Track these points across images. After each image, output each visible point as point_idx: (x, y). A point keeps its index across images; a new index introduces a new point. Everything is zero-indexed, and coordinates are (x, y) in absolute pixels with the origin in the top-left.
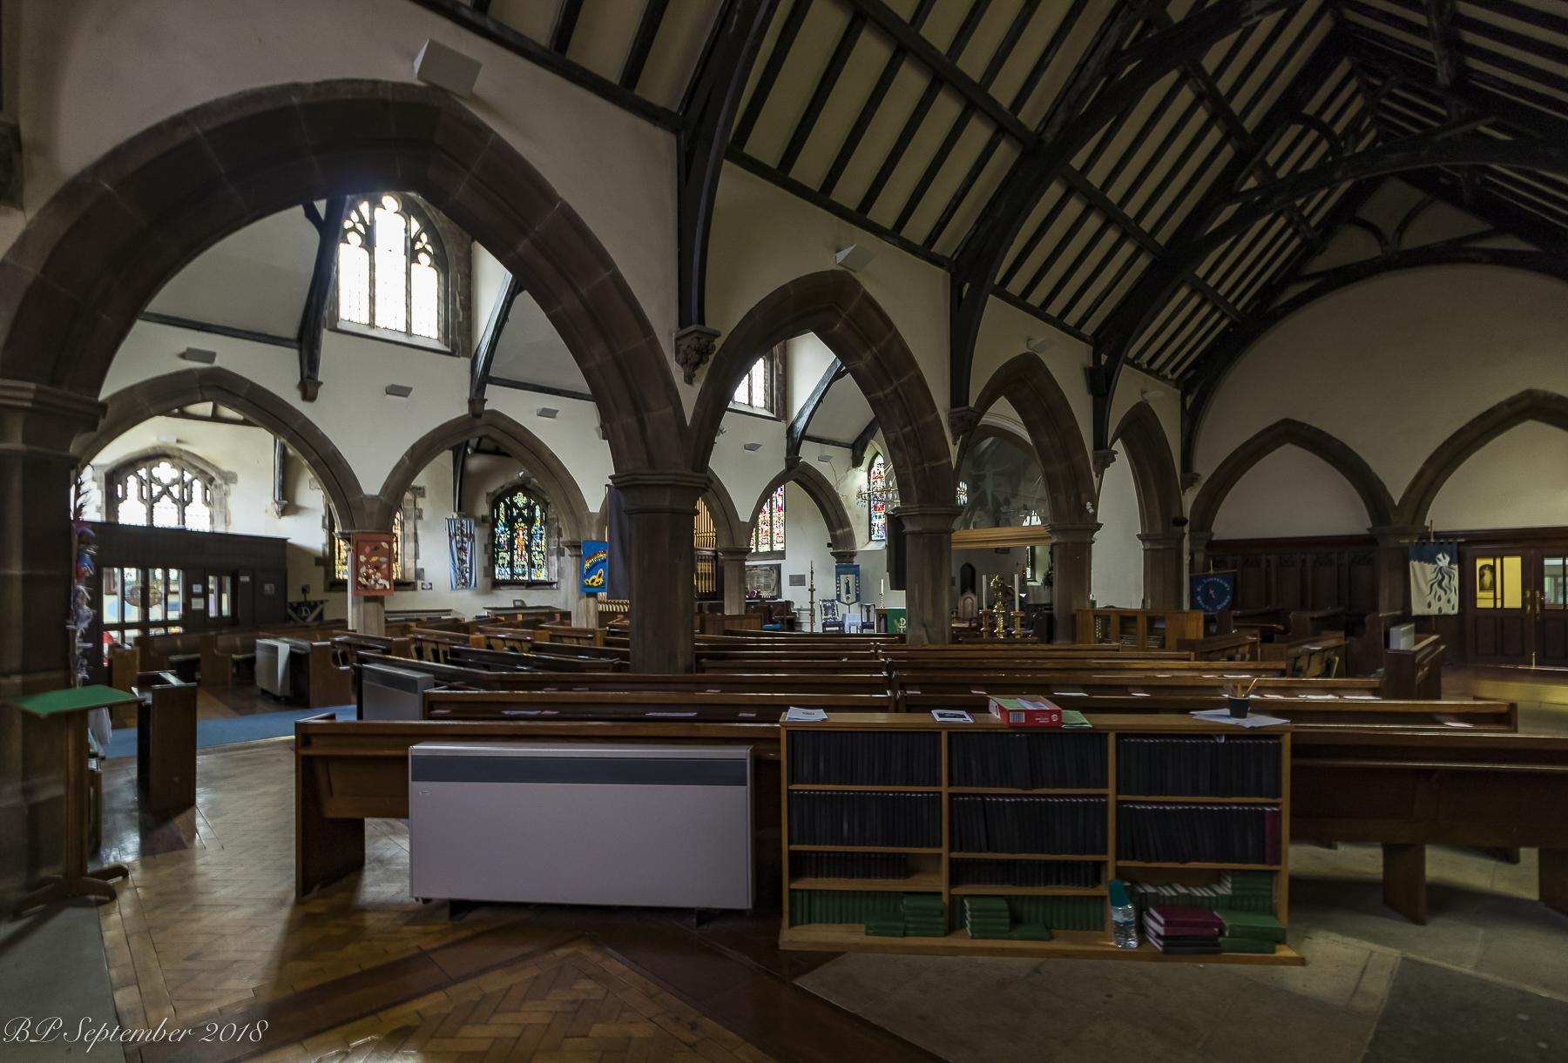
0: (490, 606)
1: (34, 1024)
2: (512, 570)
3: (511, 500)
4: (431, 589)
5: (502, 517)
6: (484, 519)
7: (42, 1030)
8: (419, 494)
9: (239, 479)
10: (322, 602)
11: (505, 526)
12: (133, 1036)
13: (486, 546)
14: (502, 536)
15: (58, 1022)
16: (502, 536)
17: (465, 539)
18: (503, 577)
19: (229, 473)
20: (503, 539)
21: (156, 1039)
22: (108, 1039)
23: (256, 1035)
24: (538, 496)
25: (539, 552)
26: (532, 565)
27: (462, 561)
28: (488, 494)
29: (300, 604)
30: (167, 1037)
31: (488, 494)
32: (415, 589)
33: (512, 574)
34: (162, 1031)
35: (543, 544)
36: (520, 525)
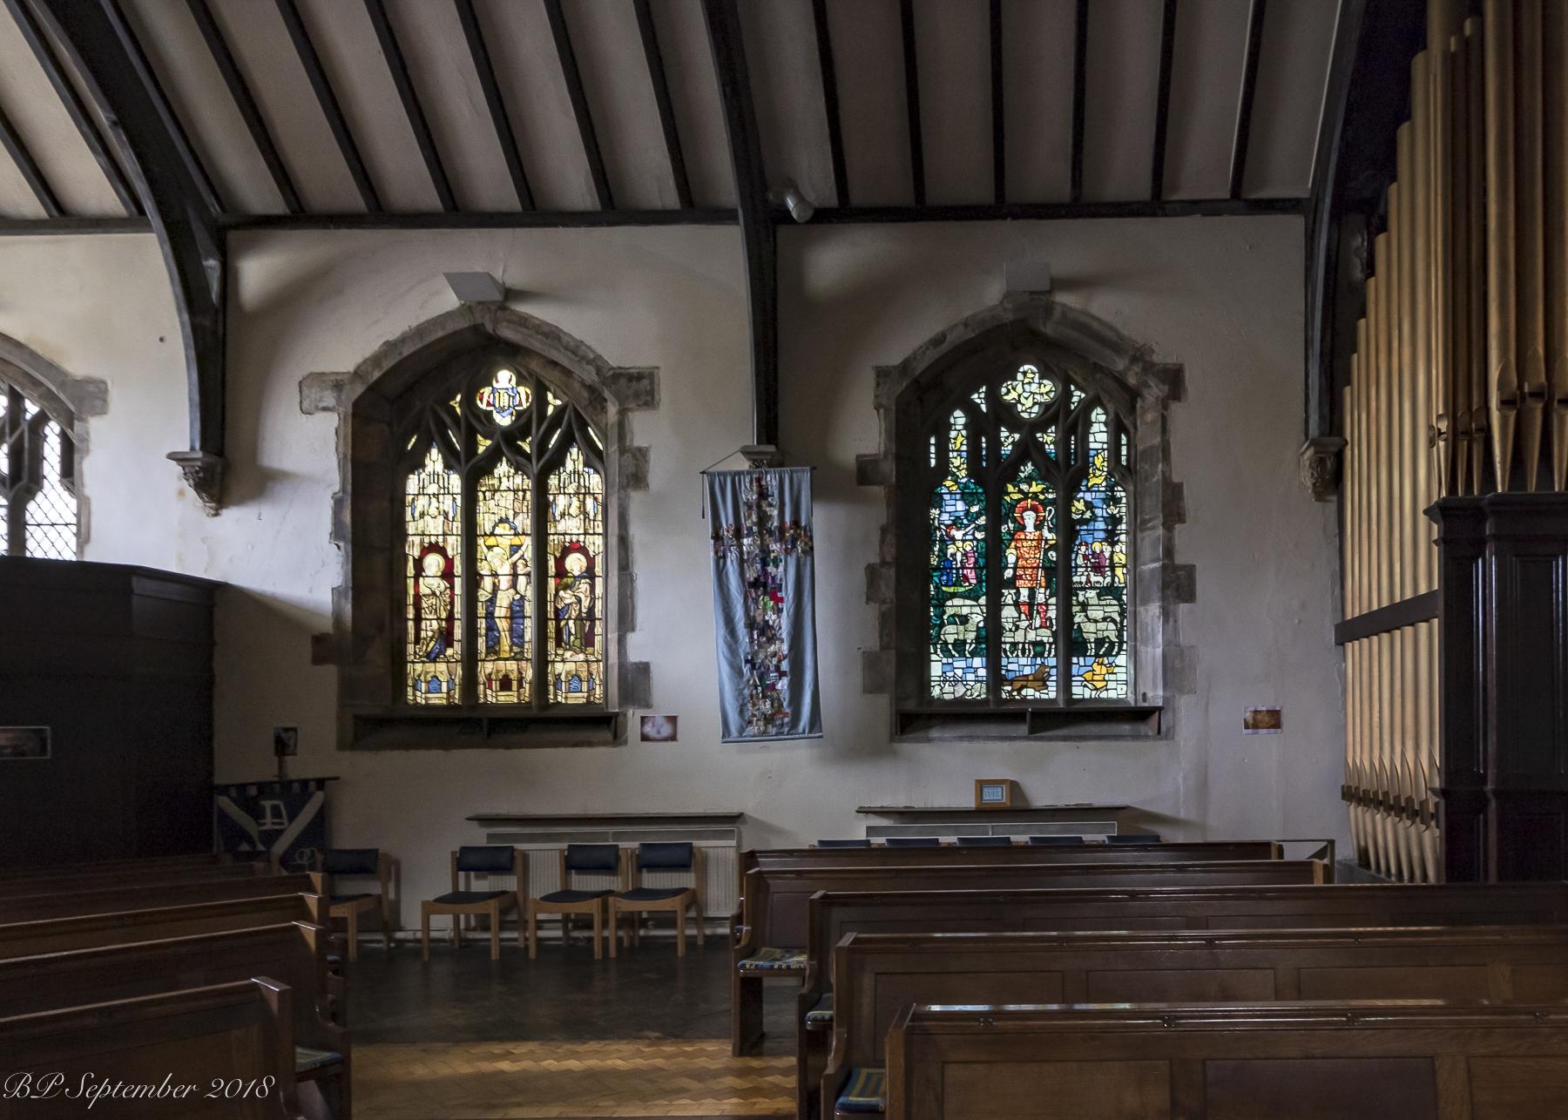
0: (877, 803)
1: (35, 1079)
2: (994, 666)
3: (994, 397)
4: (673, 738)
5: (957, 461)
6: (865, 471)
7: (43, 1086)
8: (637, 395)
9: (114, 396)
10: (321, 783)
11: (967, 497)
12: (135, 1093)
13: (872, 572)
14: (958, 535)
15: (60, 1078)
16: (958, 535)
17: (775, 547)
18: (960, 690)
19: (89, 381)
20: (963, 545)
21: (161, 1095)
22: (110, 1095)
23: (262, 1091)
24: (1097, 368)
25: (1104, 592)
26: (1071, 643)
27: (766, 632)
28: (882, 374)
29: (264, 789)
30: (171, 1092)
31: (882, 374)
32: (617, 738)
33: (996, 677)
34: (166, 1088)
35: (1120, 558)
36: (1029, 486)
